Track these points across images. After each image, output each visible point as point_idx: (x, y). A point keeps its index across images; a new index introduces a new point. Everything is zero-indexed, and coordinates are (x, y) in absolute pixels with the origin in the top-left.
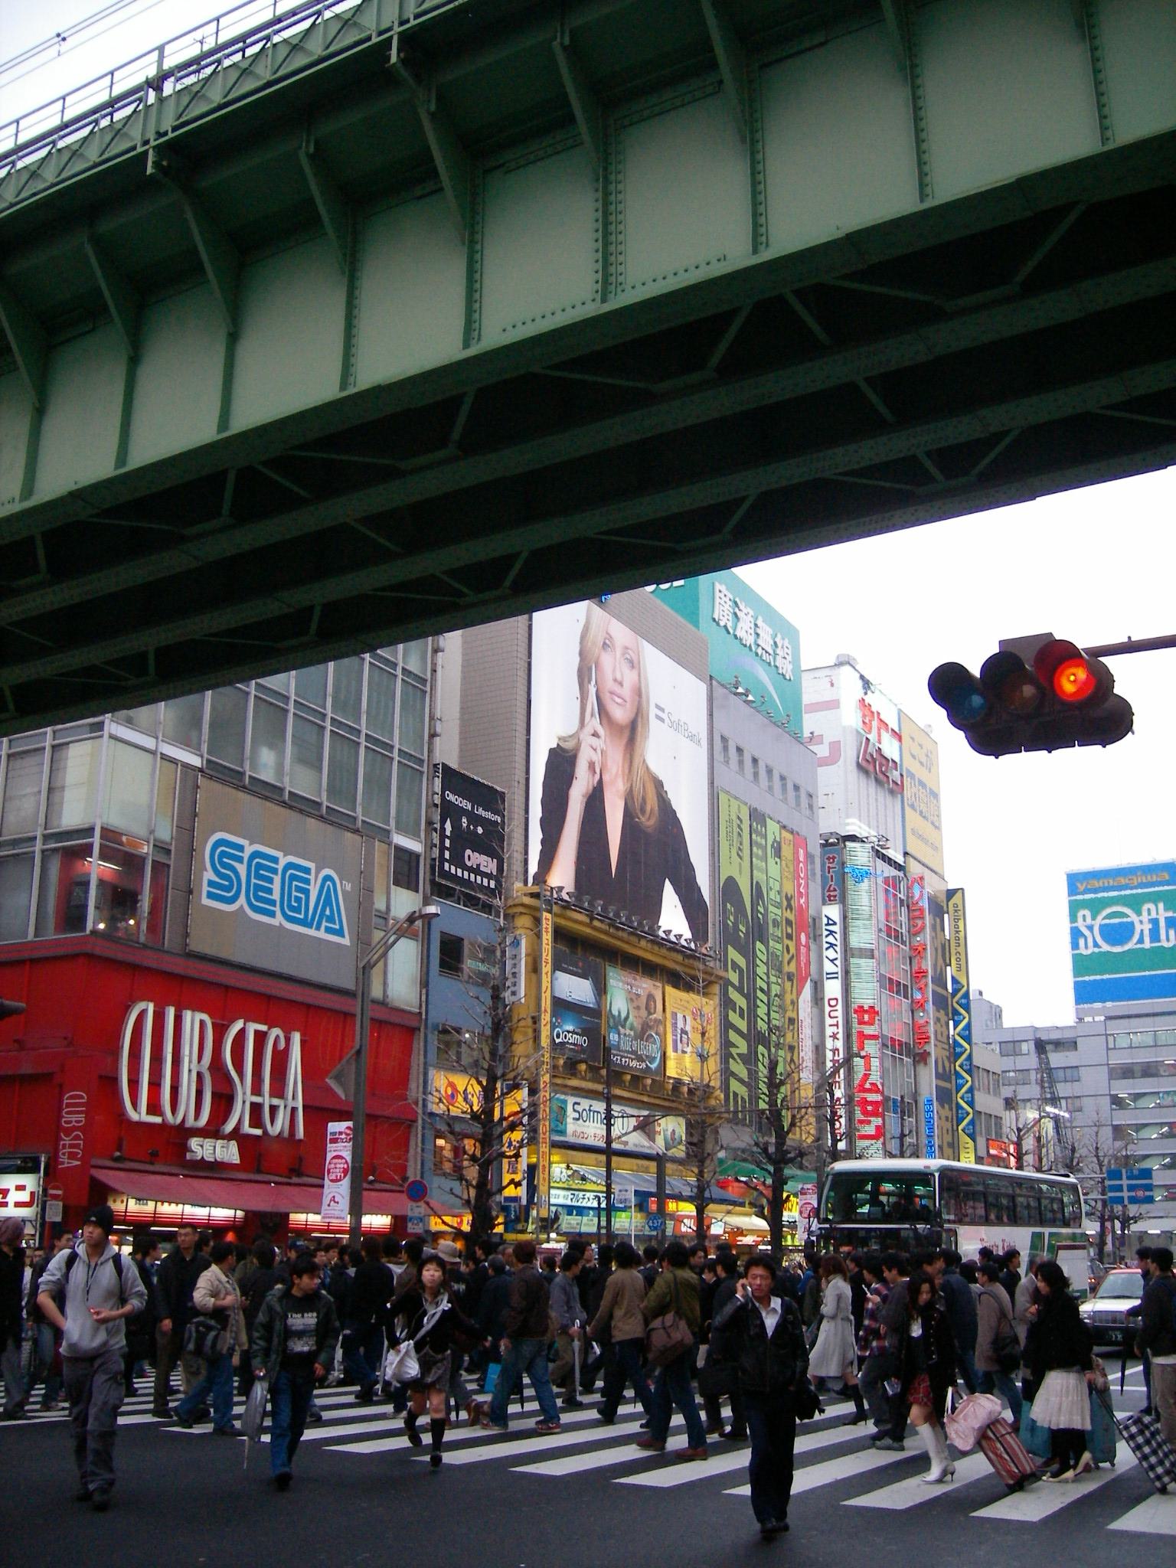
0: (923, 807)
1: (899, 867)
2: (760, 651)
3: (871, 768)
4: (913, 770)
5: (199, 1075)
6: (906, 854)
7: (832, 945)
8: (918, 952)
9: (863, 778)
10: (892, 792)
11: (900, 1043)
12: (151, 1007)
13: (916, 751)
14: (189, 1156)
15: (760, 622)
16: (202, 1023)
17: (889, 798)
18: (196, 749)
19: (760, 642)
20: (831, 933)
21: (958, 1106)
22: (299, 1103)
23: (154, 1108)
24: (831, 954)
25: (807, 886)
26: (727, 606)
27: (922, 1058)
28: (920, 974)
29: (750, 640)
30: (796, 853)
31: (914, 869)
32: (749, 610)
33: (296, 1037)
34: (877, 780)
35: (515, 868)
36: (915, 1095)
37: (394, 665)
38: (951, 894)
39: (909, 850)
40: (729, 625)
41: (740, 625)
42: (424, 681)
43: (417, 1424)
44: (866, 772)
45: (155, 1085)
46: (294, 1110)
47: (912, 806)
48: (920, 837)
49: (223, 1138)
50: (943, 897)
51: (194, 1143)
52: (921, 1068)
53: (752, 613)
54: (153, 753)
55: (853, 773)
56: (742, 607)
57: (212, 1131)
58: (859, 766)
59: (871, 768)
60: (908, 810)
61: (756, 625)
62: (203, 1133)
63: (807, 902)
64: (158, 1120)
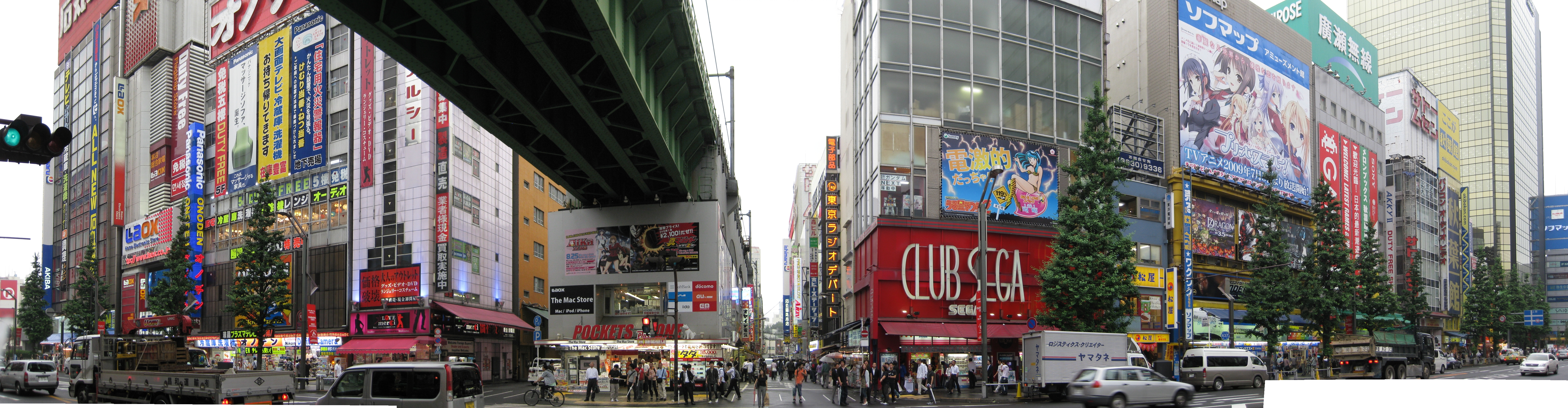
0: (1449, 148)
1: (1435, 175)
2: (1350, 56)
3: (1419, 124)
4: (1444, 129)
5: (952, 276)
6: (1438, 168)
7: (1390, 206)
8: (1443, 213)
9: (1414, 130)
10: (1432, 139)
11: (1433, 255)
12: (917, 247)
13: (1446, 121)
14: (949, 314)
15: (1350, 39)
16: (952, 251)
17: (1430, 142)
18: (938, 117)
19: (1350, 50)
20: (1390, 200)
21: (1463, 284)
22: (1021, 285)
23: (925, 291)
24: (1389, 210)
25: (1376, 177)
26: (1328, 28)
27: (1443, 262)
28: (1443, 224)
29: (1344, 49)
30: (1370, 161)
31: (1442, 175)
32: (1342, 32)
33: (1017, 253)
34: (1423, 131)
35: (1172, 159)
36: (1440, 278)
37: (1076, 55)
38: (1462, 189)
39: (1440, 166)
40: (1329, 39)
41: (1336, 40)
42: (1099, 62)
43: (1197, 133)
44: (1416, 126)
45: (924, 282)
46: (1017, 289)
47: (1443, 147)
48: (1447, 162)
49: (971, 304)
50: (1459, 191)
51: (951, 307)
52: (1442, 266)
53: (1345, 34)
54: (908, 124)
55: (1408, 126)
56: (1338, 29)
57: (964, 300)
58: (1412, 123)
59: (1419, 124)
60: (1440, 148)
61: (1348, 42)
62: (957, 302)
63: (1376, 185)
64: (927, 298)
